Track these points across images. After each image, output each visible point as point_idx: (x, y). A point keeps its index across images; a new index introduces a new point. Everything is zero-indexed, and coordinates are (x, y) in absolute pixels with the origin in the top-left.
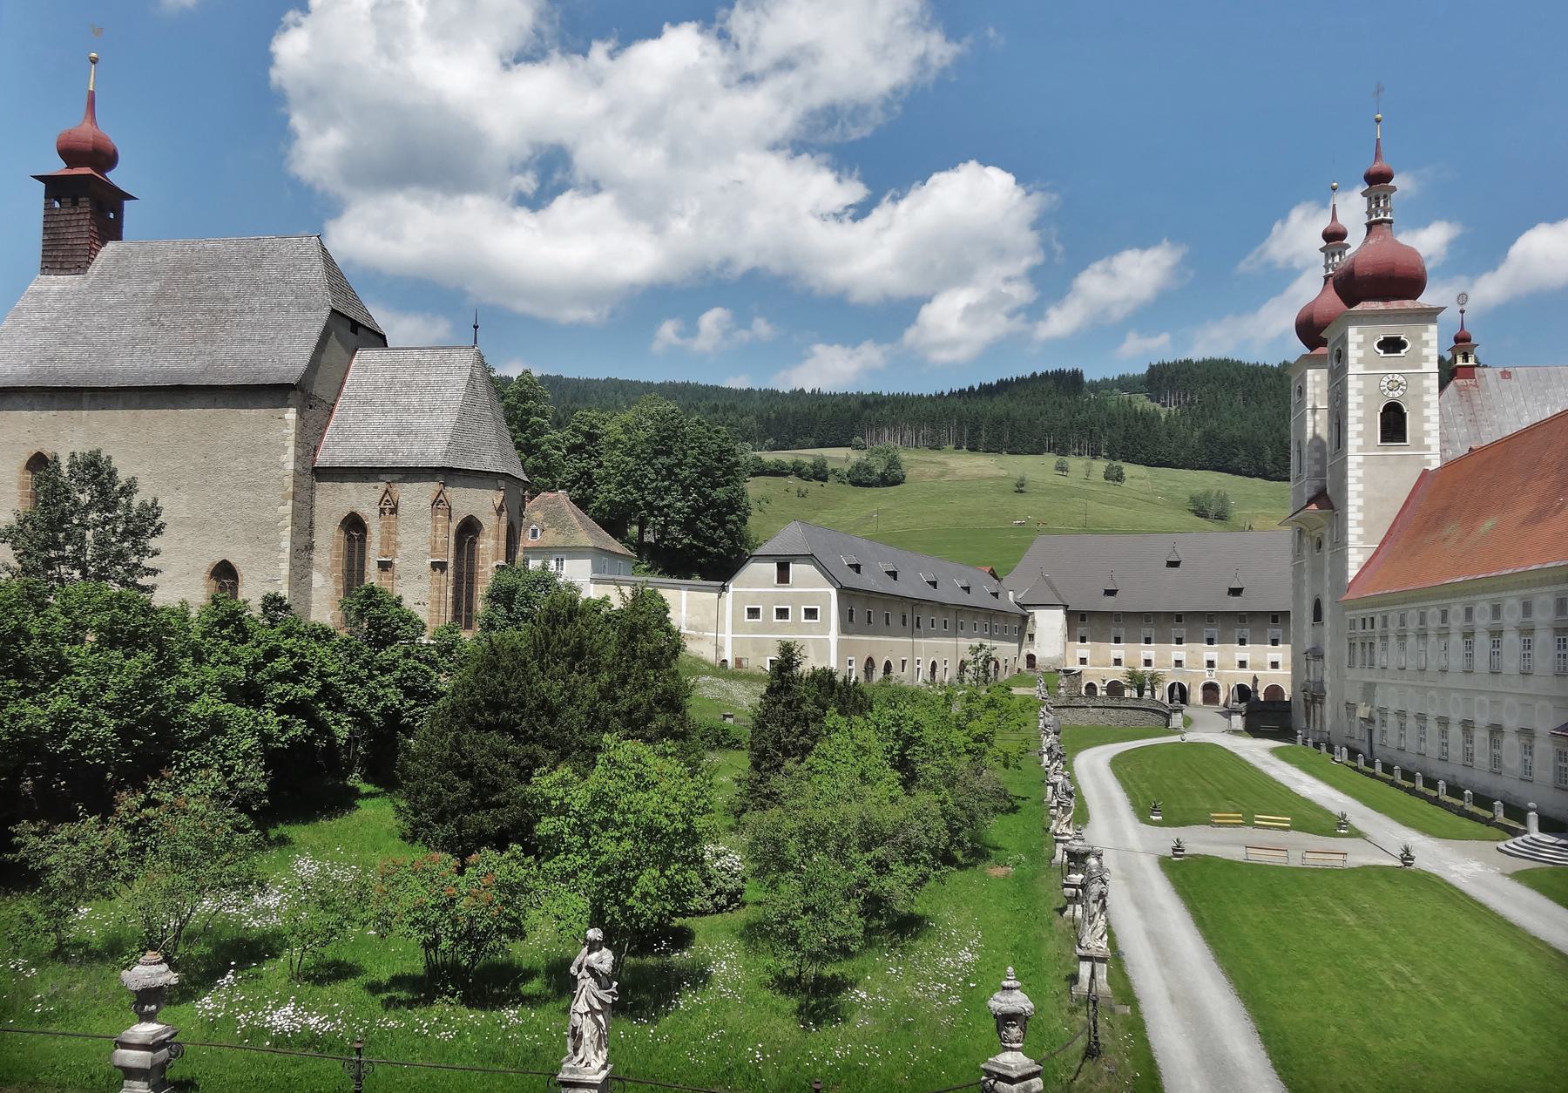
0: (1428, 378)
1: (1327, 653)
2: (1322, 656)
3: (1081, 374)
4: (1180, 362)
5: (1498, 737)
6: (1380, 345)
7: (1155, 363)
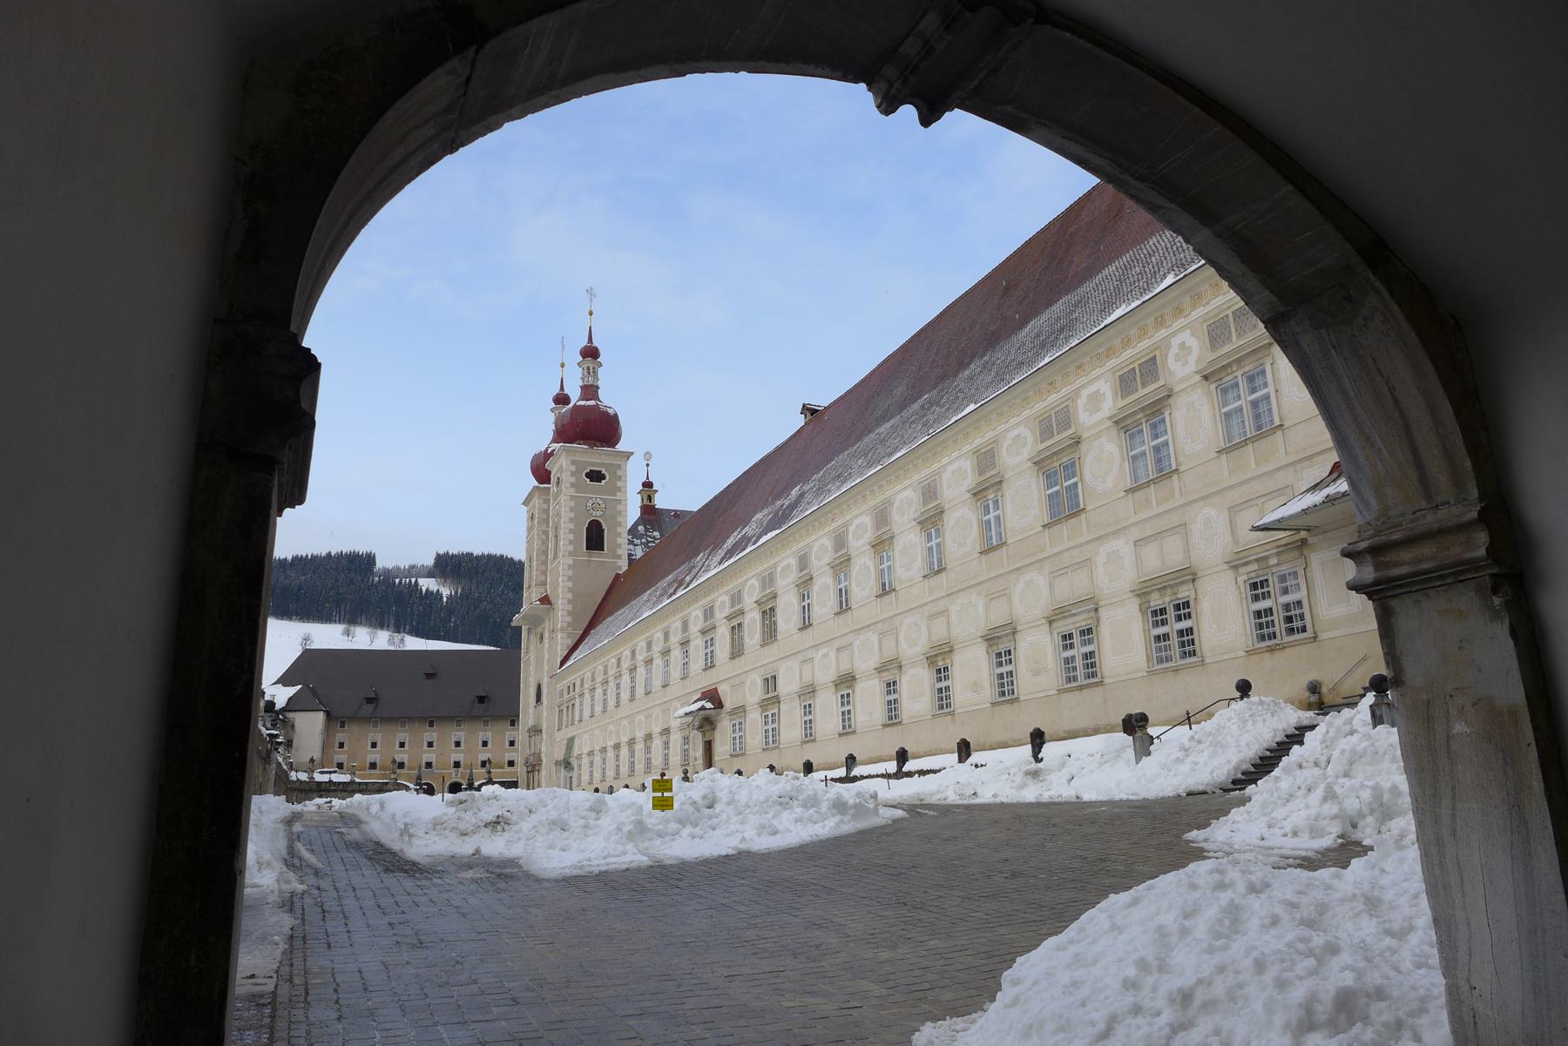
2: (541, 731)
3: (374, 555)
6: (588, 475)
7: (441, 552)
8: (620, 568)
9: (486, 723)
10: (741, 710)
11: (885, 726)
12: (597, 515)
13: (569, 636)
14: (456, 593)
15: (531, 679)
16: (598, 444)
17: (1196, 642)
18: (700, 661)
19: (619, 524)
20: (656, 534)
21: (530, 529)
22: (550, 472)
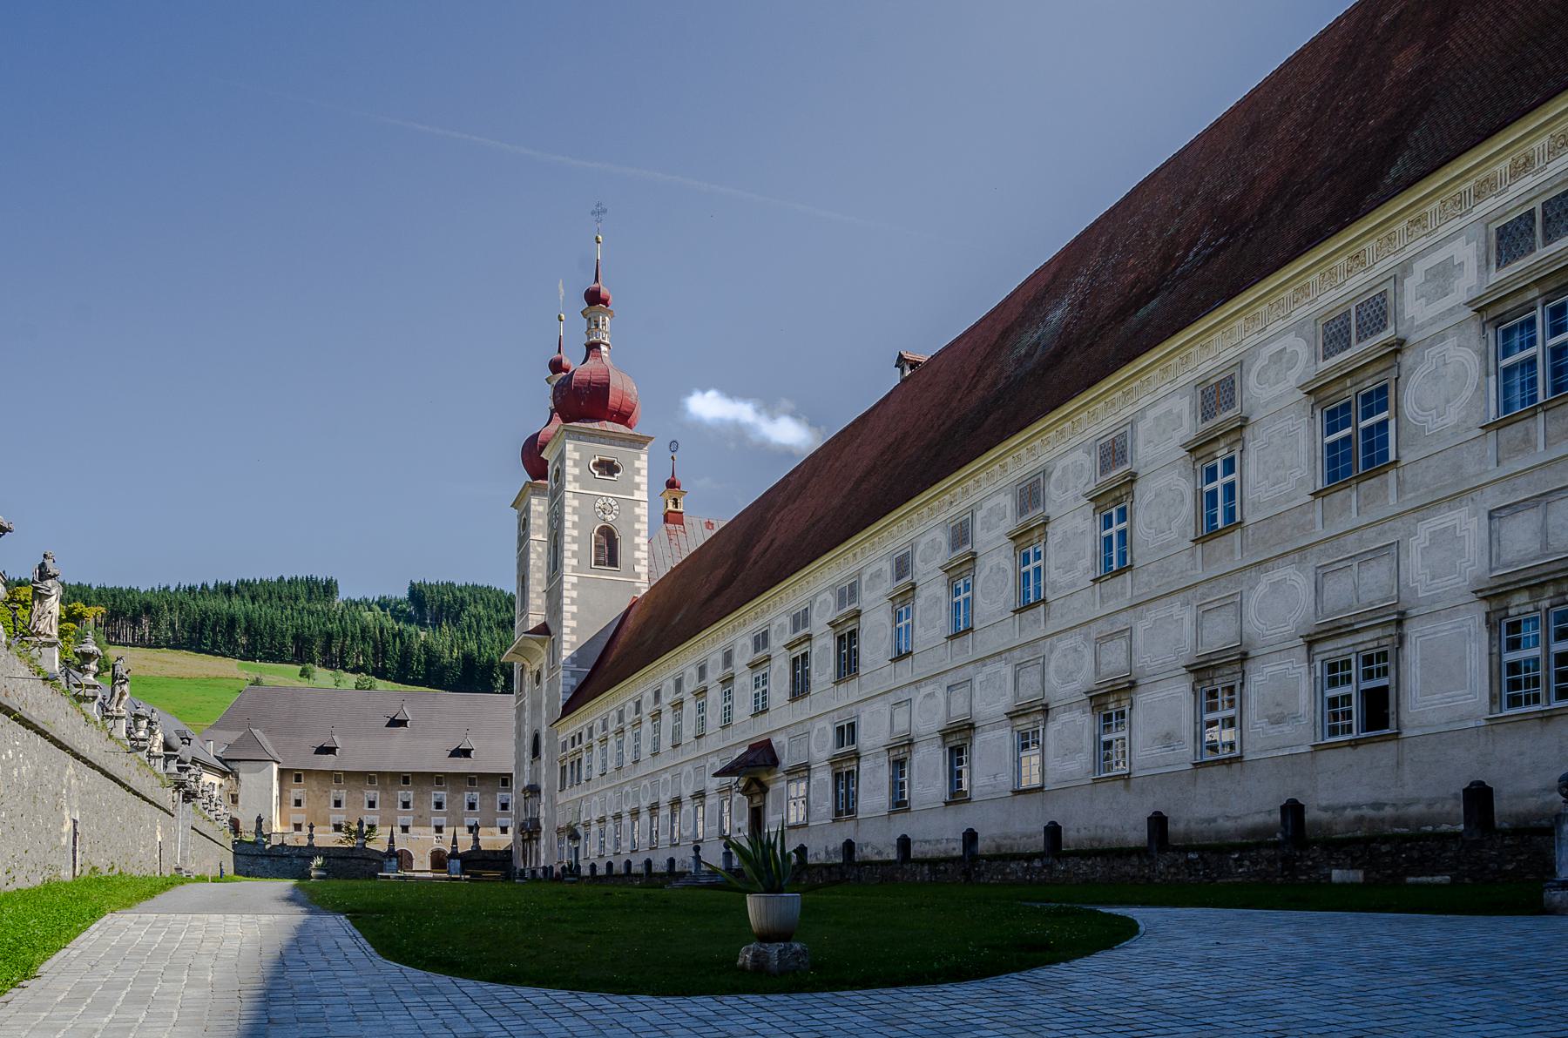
0: (639, 506)
1: (543, 786)
13: (573, 674)
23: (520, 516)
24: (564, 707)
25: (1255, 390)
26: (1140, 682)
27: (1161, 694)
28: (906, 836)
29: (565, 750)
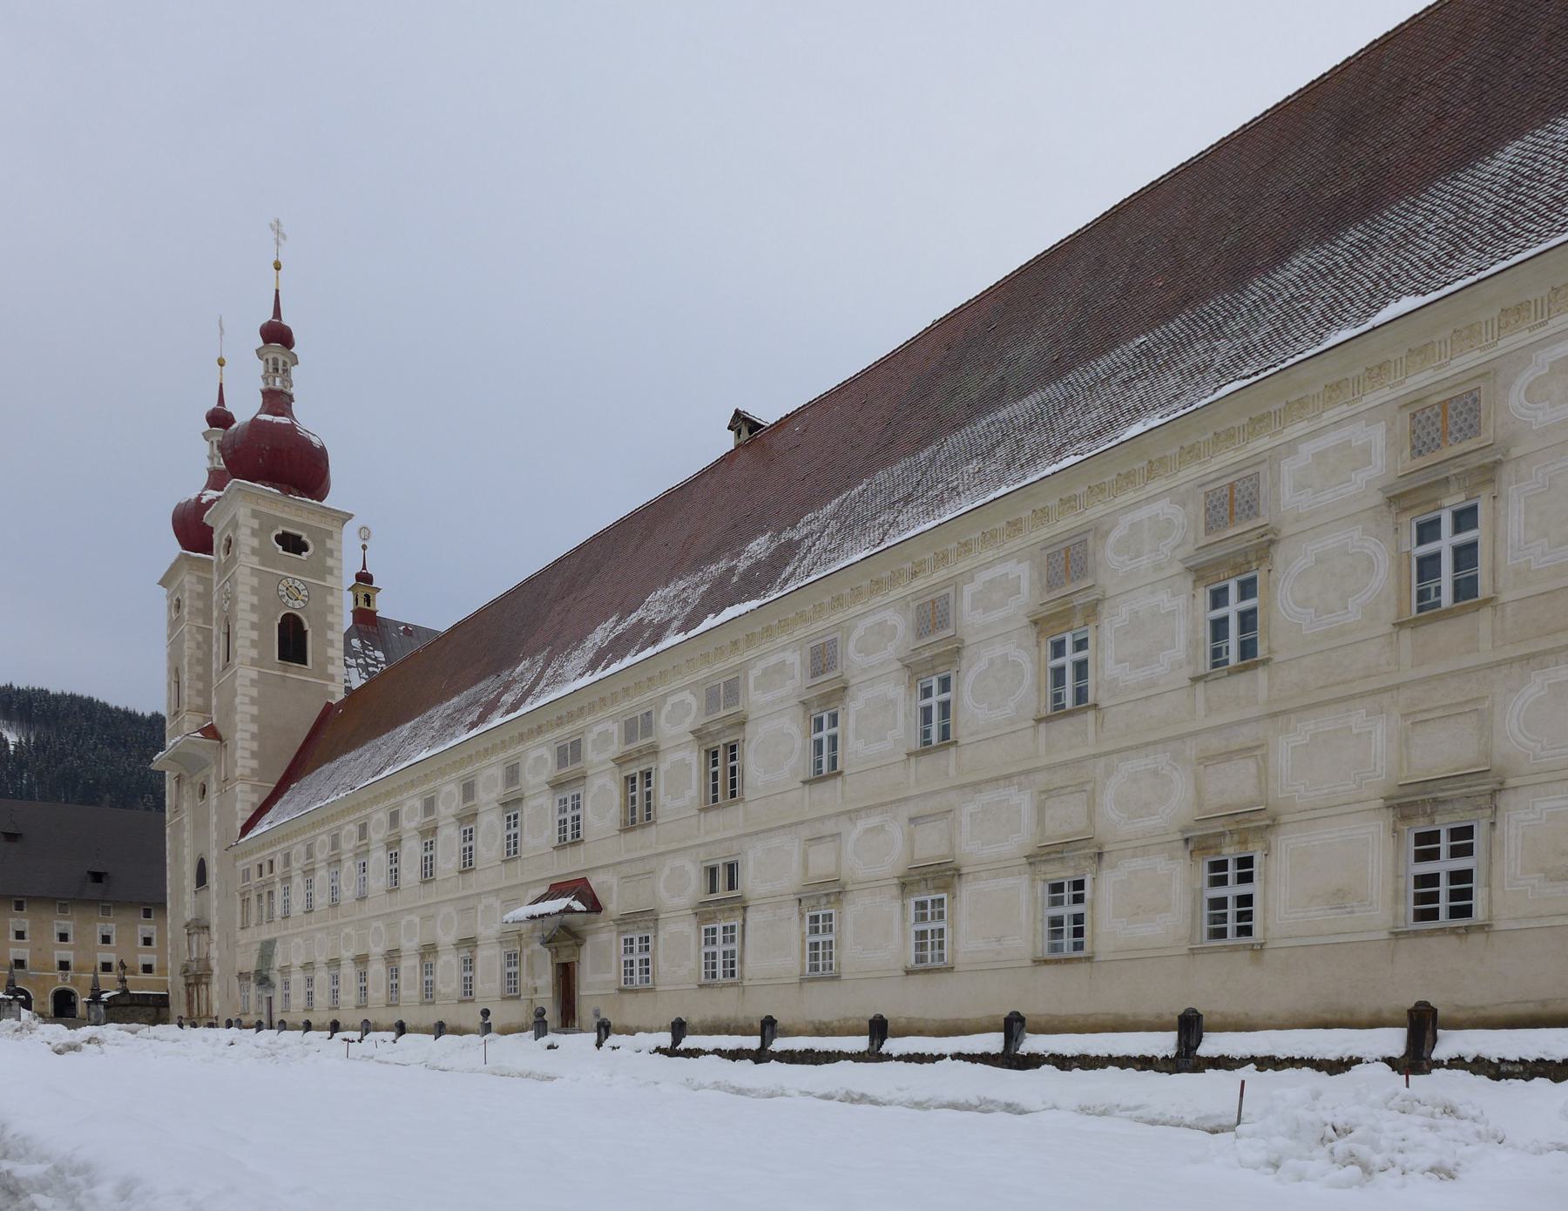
1: (214, 921)
2: (208, 928)
4: (33, 690)
5: (430, 959)
6: (280, 539)
8: (332, 694)
9: (106, 911)
10: (647, 917)
11: (1038, 962)
12: (295, 606)
13: (254, 789)
14: (28, 740)
15: (186, 851)
16: (295, 491)
17: (1086, 933)
18: (326, 895)
19: (331, 627)
20: (379, 654)
21: (174, 624)
22: (211, 530)
23: (170, 596)
24: (242, 828)
25: (1523, 410)
26: (1284, 819)
27: (1327, 836)
28: (771, 1017)
29: (248, 880)
